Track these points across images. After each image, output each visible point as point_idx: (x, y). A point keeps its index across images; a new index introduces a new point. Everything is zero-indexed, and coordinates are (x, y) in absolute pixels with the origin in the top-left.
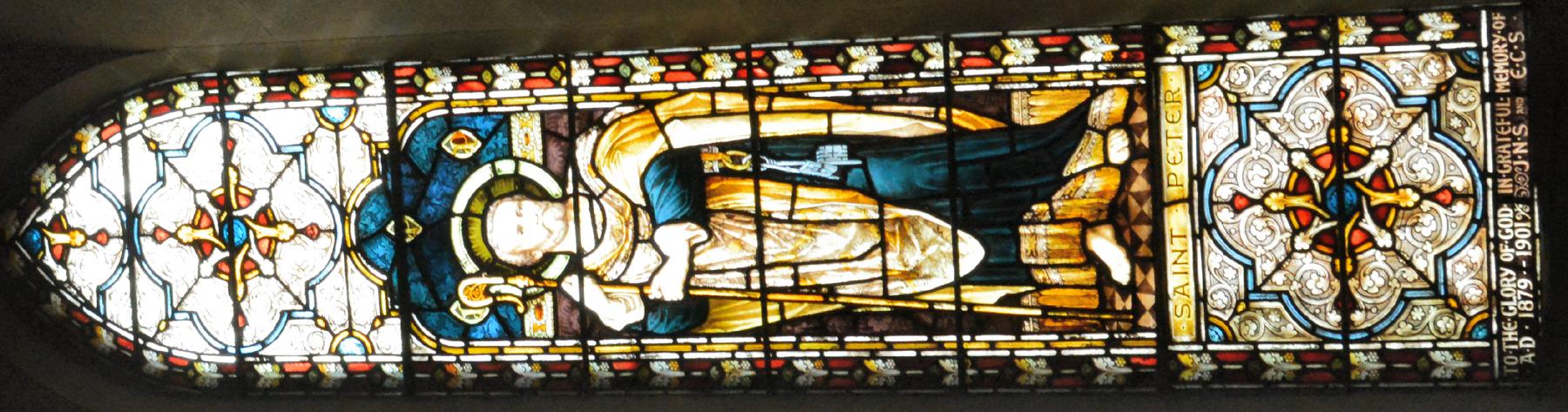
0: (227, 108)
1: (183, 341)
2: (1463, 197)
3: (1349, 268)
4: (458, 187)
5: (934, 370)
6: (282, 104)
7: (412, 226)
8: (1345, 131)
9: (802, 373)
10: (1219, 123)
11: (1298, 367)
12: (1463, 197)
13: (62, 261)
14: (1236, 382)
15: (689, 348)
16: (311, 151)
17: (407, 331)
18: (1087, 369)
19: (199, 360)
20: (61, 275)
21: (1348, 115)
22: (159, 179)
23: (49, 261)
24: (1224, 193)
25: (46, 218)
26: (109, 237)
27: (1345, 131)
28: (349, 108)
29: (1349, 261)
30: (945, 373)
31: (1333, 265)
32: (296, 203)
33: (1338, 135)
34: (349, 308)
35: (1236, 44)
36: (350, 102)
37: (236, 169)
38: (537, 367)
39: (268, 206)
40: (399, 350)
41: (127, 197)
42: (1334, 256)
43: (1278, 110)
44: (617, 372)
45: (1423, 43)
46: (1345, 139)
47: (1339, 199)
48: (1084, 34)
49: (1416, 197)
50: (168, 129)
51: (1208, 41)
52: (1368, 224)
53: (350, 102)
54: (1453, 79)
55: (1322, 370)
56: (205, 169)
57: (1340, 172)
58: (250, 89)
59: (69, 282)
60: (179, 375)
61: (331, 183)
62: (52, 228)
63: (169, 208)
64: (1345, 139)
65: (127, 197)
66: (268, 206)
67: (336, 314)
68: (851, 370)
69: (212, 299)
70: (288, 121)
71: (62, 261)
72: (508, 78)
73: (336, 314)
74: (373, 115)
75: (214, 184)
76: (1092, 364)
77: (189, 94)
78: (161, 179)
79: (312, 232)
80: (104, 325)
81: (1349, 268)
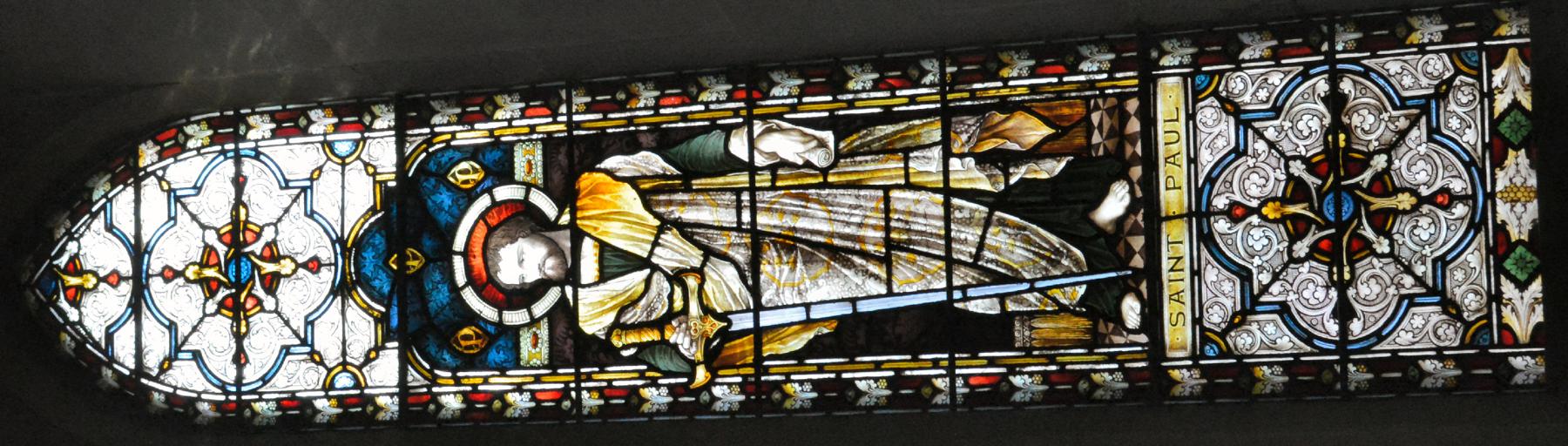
0: (241, 145)
1: (185, 378)
2: (1462, 199)
3: (1347, 276)
4: (463, 212)
5: (1413, 373)
6: (284, 141)
7: (415, 258)
8: (1342, 137)
9: (1019, 389)
10: (1218, 131)
11: (602, 402)
12: (1462, 199)
13: (76, 304)
14: (984, 405)
15: (595, 377)
16: (317, 183)
17: (404, 362)
18: (927, 391)
19: (199, 399)
20: (73, 315)
21: (1345, 120)
22: (170, 218)
23: (64, 304)
24: (1220, 203)
25: (63, 261)
26: (161, 274)
27: (1342, 137)
28: (357, 142)
29: (1347, 269)
30: (938, 391)
31: (1330, 273)
32: (302, 238)
33: (1336, 140)
34: (344, 342)
35: (1311, 47)
36: (357, 136)
37: (245, 206)
38: (334, 402)
39: (274, 242)
40: (395, 381)
41: (138, 236)
42: (1330, 265)
43: (1276, 118)
44: (972, 388)
45: (1412, 45)
46: (1342, 144)
47: (1338, 205)
48: (1243, 31)
49: (1265, 211)
50: (182, 172)
51: (808, 83)
52: (259, 291)
53: (357, 136)
54: (1452, 78)
55: (1310, 379)
56: (216, 206)
57: (1338, 179)
58: (260, 127)
59: (80, 323)
60: (182, 408)
61: (332, 215)
62: (66, 271)
63: (178, 247)
64: (1342, 144)
65: (138, 236)
66: (274, 242)
67: (319, 343)
68: (627, 398)
69: (216, 336)
70: (297, 157)
71: (76, 304)
72: (509, 109)
73: (319, 343)
74: (383, 152)
75: (223, 219)
76: (312, 406)
77: (198, 134)
78: (172, 218)
79: (314, 265)
80: (109, 366)
81: (1347, 276)
